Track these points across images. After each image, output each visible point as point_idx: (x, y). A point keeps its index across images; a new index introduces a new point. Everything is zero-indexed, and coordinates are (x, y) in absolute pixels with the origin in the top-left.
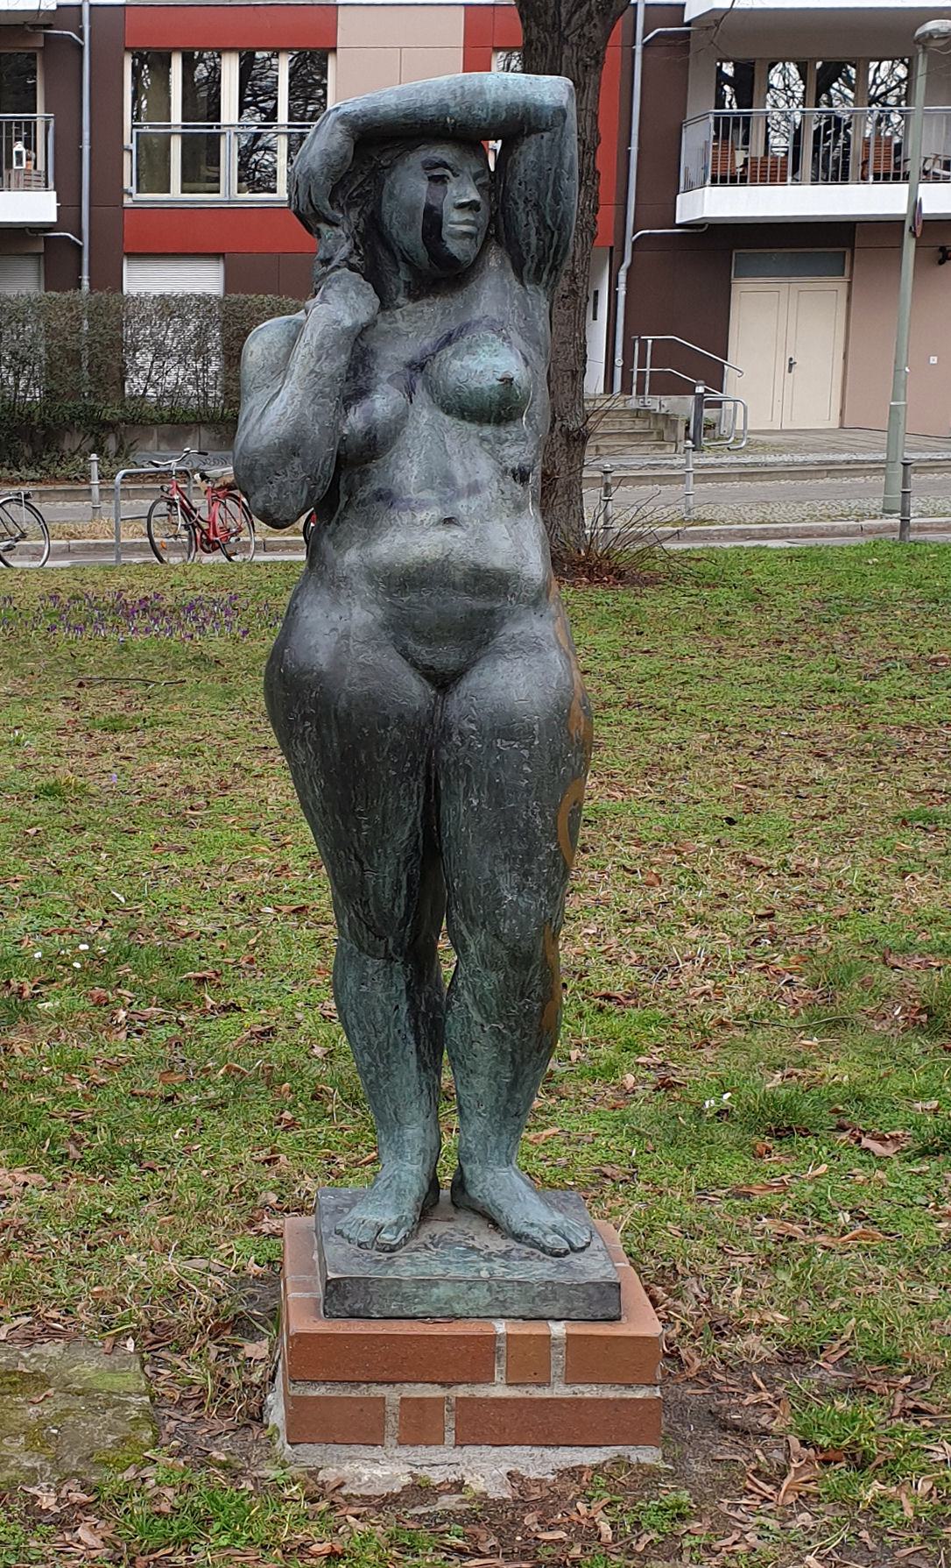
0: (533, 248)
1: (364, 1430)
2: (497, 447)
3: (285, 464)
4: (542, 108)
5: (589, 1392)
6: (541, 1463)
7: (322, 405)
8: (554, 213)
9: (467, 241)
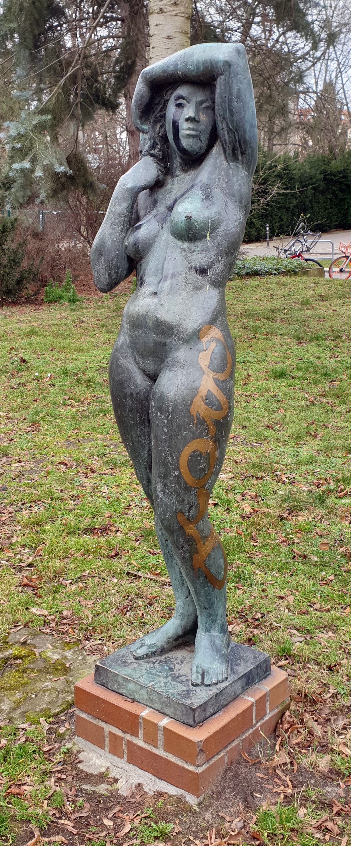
0: (227, 141)
1: (96, 739)
2: (189, 254)
3: (98, 259)
4: (217, 62)
5: (172, 758)
6: (153, 784)
7: (114, 229)
8: (232, 121)
9: (191, 140)
